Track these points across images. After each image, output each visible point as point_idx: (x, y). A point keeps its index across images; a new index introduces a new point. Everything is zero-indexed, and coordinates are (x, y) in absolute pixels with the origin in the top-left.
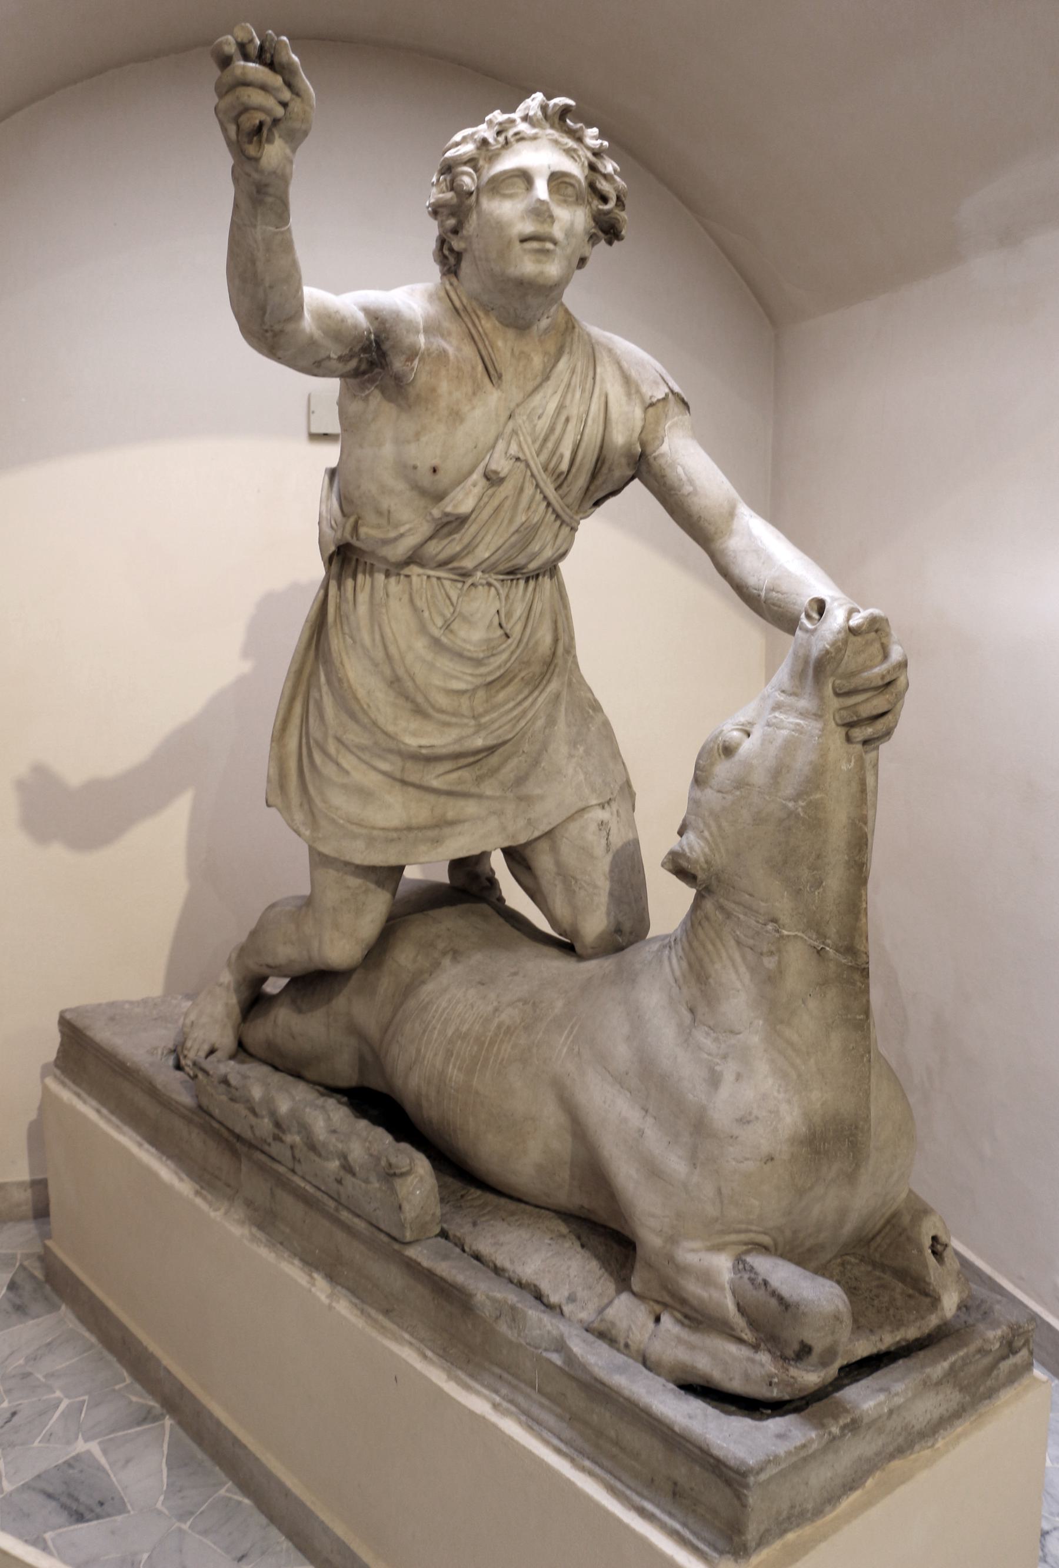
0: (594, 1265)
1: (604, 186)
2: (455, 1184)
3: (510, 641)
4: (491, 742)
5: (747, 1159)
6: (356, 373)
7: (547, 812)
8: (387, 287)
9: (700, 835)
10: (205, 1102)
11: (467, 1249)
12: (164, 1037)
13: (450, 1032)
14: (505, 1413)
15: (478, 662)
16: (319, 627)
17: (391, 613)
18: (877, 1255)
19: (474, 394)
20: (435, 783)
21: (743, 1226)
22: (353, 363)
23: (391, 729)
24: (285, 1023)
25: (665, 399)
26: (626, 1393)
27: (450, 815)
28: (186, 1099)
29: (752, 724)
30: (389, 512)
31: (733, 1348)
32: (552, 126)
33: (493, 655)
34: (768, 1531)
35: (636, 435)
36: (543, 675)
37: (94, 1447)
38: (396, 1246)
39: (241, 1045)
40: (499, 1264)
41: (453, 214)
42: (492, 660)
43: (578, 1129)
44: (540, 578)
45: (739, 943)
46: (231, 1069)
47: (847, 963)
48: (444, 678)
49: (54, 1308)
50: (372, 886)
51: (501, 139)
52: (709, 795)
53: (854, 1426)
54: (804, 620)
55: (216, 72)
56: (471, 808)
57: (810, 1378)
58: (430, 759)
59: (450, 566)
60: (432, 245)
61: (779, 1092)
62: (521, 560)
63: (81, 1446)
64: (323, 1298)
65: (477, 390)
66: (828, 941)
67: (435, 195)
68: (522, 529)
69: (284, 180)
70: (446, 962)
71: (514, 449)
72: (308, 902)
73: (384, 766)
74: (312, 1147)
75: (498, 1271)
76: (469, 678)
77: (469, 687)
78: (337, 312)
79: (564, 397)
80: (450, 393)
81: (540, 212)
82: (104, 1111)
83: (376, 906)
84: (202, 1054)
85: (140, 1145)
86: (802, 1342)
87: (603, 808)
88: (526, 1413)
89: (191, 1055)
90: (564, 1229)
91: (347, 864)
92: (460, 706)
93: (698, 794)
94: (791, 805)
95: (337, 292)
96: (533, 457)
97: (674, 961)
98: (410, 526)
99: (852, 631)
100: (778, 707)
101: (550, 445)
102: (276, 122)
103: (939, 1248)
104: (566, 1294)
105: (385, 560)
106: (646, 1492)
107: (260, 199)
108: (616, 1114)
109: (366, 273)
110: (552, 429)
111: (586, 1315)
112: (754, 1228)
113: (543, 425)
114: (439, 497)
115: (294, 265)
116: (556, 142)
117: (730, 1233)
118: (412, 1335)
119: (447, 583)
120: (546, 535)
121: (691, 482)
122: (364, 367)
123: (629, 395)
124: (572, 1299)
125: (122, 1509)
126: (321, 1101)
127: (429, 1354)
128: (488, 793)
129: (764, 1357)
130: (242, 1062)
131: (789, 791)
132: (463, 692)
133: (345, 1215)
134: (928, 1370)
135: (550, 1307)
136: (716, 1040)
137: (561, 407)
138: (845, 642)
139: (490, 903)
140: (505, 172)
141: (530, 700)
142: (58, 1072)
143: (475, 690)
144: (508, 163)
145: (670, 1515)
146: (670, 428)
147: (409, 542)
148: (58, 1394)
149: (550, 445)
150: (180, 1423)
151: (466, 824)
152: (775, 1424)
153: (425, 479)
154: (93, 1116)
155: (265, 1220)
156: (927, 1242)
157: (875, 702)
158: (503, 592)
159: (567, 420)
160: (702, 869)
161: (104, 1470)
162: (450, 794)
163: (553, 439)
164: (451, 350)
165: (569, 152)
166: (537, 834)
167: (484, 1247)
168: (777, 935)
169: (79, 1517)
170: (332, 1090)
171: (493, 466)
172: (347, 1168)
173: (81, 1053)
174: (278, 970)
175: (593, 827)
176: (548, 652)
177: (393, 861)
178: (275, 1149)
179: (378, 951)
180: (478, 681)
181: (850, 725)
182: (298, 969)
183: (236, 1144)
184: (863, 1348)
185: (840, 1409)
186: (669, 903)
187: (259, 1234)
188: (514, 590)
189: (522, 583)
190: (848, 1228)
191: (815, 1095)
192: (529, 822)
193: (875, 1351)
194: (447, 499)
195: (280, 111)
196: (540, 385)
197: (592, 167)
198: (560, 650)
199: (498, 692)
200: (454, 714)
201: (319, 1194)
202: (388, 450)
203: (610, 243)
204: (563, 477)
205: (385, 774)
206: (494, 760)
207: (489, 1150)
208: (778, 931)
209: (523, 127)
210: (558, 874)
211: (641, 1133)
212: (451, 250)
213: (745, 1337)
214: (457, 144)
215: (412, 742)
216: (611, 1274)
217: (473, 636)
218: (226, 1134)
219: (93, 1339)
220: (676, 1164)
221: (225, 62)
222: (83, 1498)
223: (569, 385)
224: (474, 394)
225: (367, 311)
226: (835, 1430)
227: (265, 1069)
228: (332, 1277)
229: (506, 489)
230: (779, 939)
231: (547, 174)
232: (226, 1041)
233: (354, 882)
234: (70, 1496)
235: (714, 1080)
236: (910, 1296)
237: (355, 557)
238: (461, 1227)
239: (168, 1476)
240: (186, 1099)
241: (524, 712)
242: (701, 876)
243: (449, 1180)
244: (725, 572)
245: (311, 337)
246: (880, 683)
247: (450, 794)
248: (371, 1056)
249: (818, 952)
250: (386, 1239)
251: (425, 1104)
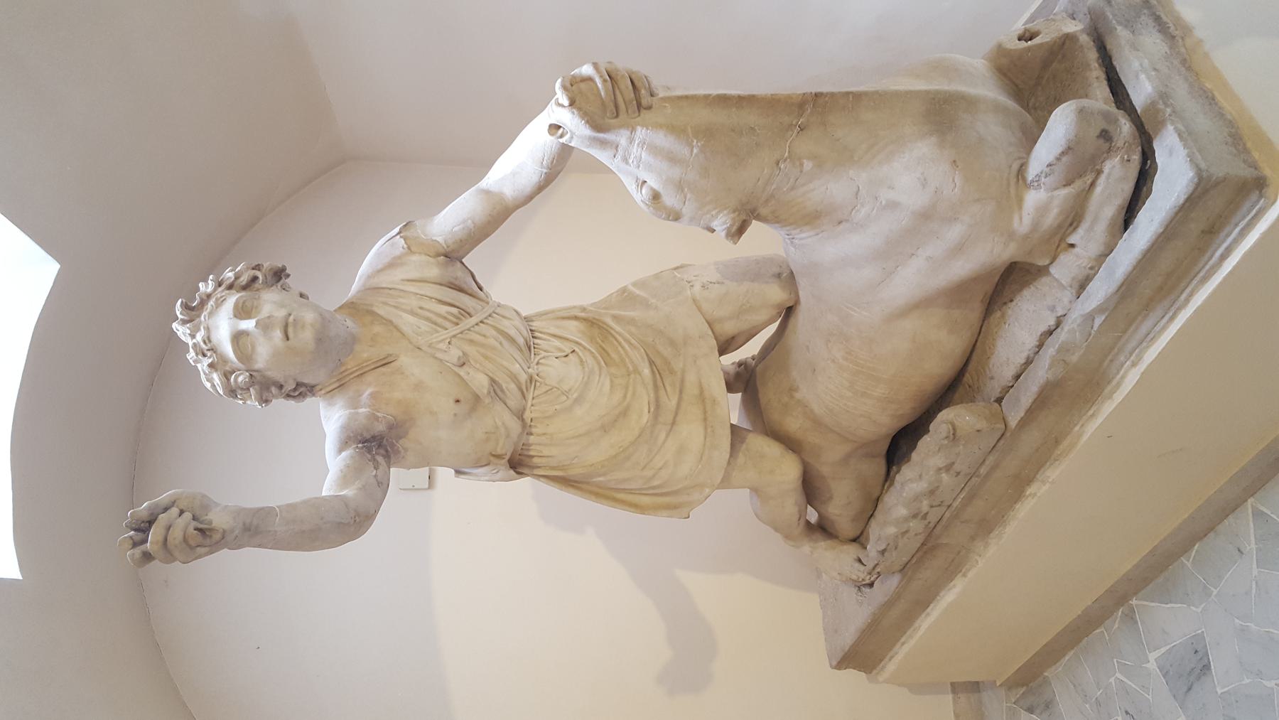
0: (1026, 293)
1: (244, 279)
2: (961, 390)
4: (647, 364)
6: (387, 456)
7: (697, 326)
8: (324, 435)
9: (714, 217)
10: (898, 567)
12: (849, 593)
13: (849, 394)
14: (1140, 358)
16: (566, 482)
17: (557, 437)
20: (674, 402)
22: (380, 459)
24: (840, 508)
25: (405, 239)
26: (1130, 268)
27: (696, 392)
28: (894, 581)
29: (637, 179)
31: (1098, 189)
32: (199, 316)
34: (1244, 161)
36: (600, 327)
37: (1152, 656)
38: (1008, 434)
39: (854, 540)
40: (1023, 361)
41: (268, 389)
43: (922, 305)
45: (793, 188)
46: (873, 548)
47: (810, 111)
49: (1046, 681)
50: (744, 446)
51: (209, 354)
52: (687, 210)
53: (1164, 96)
54: (563, 140)
55: (156, 563)
56: (691, 378)
57: (1125, 127)
60: (292, 402)
62: (521, 341)
63: (1152, 665)
64: (1045, 488)
67: (253, 403)
69: (239, 511)
71: (443, 346)
72: (755, 490)
73: (663, 436)
74: (932, 492)
75: (1029, 362)
79: (405, 311)
81: (265, 326)
82: (903, 640)
83: (760, 444)
84: (862, 568)
85: (928, 614)
86: (1098, 137)
89: (862, 576)
90: (998, 314)
91: (729, 463)
93: (685, 219)
97: (803, 235)
98: (500, 418)
99: (572, 104)
100: (625, 160)
101: (440, 320)
102: (194, 518)
103: (1027, 35)
105: (520, 436)
106: (1208, 254)
107: (255, 530)
108: (914, 277)
109: (314, 447)
110: (428, 319)
111: (1067, 295)
113: (425, 326)
114: (477, 398)
115: (304, 502)
116: (211, 314)
119: (537, 393)
120: (505, 325)
121: (464, 221)
122: (382, 451)
124: (1053, 309)
125: (1201, 637)
126: (897, 484)
127: (1091, 412)
129: (1107, 167)
130: (867, 539)
131: (686, 151)
132: (612, 381)
133: (983, 471)
134: (1123, 42)
135: (1058, 325)
136: (862, 205)
137: (413, 313)
138: (579, 109)
139: (756, 365)
142: (875, 672)
144: (228, 350)
145: (1228, 235)
148: (1112, 680)
149: (440, 320)
150: (1135, 594)
152: (1160, 157)
154: (906, 648)
155: (986, 527)
156: (1024, 44)
158: (544, 354)
161: (1169, 651)
162: (681, 392)
163: (435, 318)
164: (369, 391)
165: (220, 303)
167: (1009, 373)
169: (1207, 667)
170: (888, 477)
171: (455, 360)
172: (948, 468)
173: (861, 655)
174: (802, 514)
177: (728, 431)
178: (933, 518)
179: (790, 443)
181: (639, 106)
182: (802, 499)
183: (928, 546)
184: (1101, 91)
185: (1152, 107)
186: (763, 240)
187: (996, 532)
190: (1011, 104)
193: (1105, 82)
194: (478, 392)
195: (188, 515)
196: (396, 327)
197: (230, 287)
198: (583, 315)
200: (627, 388)
201: (967, 489)
203: (288, 276)
205: (667, 436)
206: (658, 361)
207: (937, 368)
209: (199, 337)
211: (929, 258)
212: (295, 390)
213: (1089, 182)
214: (213, 386)
215: (645, 418)
216: (1035, 280)
218: (920, 553)
219: (1072, 652)
220: (954, 233)
221: (147, 557)
223: (396, 307)
225: (340, 451)
226: (1169, 110)
227: (873, 523)
228: (1030, 481)
229: (472, 350)
231: (236, 320)
232: (852, 551)
233: (741, 459)
235: (893, 205)
236: (1064, 56)
238: (994, 389)
240: (894, 581)
241: (626, 340)
243: (957, 395)
244: (530, 198)
248: (863, 449)
250: (1002, 442)
251: (901, 412)
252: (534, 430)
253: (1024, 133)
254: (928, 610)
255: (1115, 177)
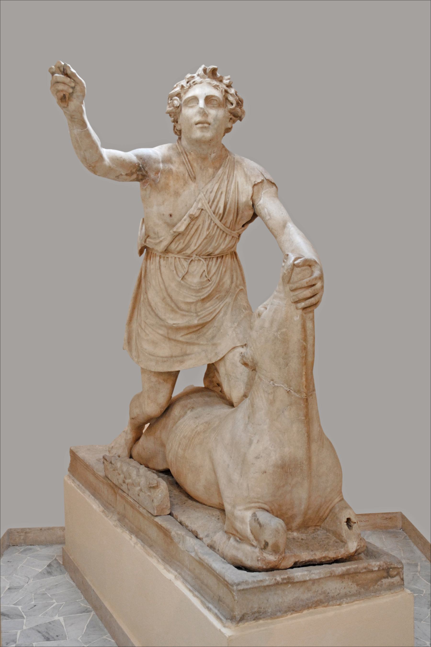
1: (231, 98)
3: (210, 283)
4: (201, 322)
5: (256, 472)
11: (178, 520)
15: (198, 291)
18: (327, 525)
19: (184, 185)
20: (181, 339)
21: (256, 500)
23: (163, 317)
25: (262, 182)
26: (206, 561)
27: (188, 352)
30: (158, 233)
32: (209, 77)
33: (203, 288)
35: (250, 197)
37: (61, 619)
38: (153, 518)
42: (203, 290)
44: (224, 258)
48: (186, 297)
49: (62, 573)
51: (188, 84)
56: (196, 349)
58: (178, 329)
59: (182, 253)
61: (271, 447)
63: (56, 618)
65: (185, 183)
66: (292, 388)
68: (208, 237)
70: (189, 412)
76: (194, 298)
77: (194, 301)
78: (121, 157)
80: (174, 185)
87: (243, 347)
88: (184, 578)
92: (191, 308)
94: (276, 334)
95: (126, 150)
96: (208, 208)
104: (206, 534)
112: (261, 501)
113: (213, 194)
116: (210, 83)
117: (252, 503)
118: (156, 554)
119: (182, 260)
123: (247, 181)
128: (202, 343)
132: (193, 303)
133: (141, 509)
140: (189, 98)
141: (218, 305)
143: (197, 302)
144: (190, 94)
146: (264, 193)
147: (165, 244)
148: (54, 601)
150: (97, 614)
151: (193, 355)
153: (168, 219)
157: (305, 293)
159: (222, 193)
160: (250, 361)
162: (187, 343)
165: (216, 87)
166: (219, 358)
167: (183, 518)
168: (273, 386)
175: (238, 355)
176: (228, 287)
178: (124, 487)
180: (197, 299)
181: (296, 302)
183: (115, 488)
188: (210, 263)
189: (215, 260)
191: (286, 450)
192: (216, 354)
199: (207, 303)
201: (134, 502)
202: (155, 209)
204: (221, 216)
208: (273, 384)
209: (197, 79)
210: (226, 374)
213: (254, 544)
215: (171, 322)
217: (194, 280)
218: (112, 484)
219: (74, 584)
220: (236, 477)
221: (53, 74)
222: (51, 634)
224: (184, 185)
230: (274, 387)
233: (154, 379)
234: (47, 632)
235: (250, 443)
237: (150, 251)
239: (86, 630)
242: (250, 364)
245: (110, 167)
246: (306, 285)
247: (187, 343)
249: (288, 392)
252: (162, 260)
253: (390, 589)
254: (91, 496)
255: (249, 554)
